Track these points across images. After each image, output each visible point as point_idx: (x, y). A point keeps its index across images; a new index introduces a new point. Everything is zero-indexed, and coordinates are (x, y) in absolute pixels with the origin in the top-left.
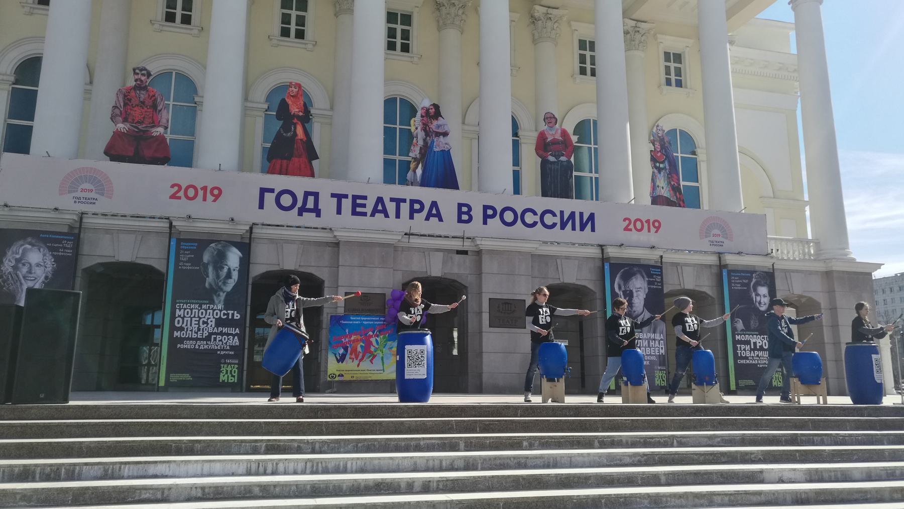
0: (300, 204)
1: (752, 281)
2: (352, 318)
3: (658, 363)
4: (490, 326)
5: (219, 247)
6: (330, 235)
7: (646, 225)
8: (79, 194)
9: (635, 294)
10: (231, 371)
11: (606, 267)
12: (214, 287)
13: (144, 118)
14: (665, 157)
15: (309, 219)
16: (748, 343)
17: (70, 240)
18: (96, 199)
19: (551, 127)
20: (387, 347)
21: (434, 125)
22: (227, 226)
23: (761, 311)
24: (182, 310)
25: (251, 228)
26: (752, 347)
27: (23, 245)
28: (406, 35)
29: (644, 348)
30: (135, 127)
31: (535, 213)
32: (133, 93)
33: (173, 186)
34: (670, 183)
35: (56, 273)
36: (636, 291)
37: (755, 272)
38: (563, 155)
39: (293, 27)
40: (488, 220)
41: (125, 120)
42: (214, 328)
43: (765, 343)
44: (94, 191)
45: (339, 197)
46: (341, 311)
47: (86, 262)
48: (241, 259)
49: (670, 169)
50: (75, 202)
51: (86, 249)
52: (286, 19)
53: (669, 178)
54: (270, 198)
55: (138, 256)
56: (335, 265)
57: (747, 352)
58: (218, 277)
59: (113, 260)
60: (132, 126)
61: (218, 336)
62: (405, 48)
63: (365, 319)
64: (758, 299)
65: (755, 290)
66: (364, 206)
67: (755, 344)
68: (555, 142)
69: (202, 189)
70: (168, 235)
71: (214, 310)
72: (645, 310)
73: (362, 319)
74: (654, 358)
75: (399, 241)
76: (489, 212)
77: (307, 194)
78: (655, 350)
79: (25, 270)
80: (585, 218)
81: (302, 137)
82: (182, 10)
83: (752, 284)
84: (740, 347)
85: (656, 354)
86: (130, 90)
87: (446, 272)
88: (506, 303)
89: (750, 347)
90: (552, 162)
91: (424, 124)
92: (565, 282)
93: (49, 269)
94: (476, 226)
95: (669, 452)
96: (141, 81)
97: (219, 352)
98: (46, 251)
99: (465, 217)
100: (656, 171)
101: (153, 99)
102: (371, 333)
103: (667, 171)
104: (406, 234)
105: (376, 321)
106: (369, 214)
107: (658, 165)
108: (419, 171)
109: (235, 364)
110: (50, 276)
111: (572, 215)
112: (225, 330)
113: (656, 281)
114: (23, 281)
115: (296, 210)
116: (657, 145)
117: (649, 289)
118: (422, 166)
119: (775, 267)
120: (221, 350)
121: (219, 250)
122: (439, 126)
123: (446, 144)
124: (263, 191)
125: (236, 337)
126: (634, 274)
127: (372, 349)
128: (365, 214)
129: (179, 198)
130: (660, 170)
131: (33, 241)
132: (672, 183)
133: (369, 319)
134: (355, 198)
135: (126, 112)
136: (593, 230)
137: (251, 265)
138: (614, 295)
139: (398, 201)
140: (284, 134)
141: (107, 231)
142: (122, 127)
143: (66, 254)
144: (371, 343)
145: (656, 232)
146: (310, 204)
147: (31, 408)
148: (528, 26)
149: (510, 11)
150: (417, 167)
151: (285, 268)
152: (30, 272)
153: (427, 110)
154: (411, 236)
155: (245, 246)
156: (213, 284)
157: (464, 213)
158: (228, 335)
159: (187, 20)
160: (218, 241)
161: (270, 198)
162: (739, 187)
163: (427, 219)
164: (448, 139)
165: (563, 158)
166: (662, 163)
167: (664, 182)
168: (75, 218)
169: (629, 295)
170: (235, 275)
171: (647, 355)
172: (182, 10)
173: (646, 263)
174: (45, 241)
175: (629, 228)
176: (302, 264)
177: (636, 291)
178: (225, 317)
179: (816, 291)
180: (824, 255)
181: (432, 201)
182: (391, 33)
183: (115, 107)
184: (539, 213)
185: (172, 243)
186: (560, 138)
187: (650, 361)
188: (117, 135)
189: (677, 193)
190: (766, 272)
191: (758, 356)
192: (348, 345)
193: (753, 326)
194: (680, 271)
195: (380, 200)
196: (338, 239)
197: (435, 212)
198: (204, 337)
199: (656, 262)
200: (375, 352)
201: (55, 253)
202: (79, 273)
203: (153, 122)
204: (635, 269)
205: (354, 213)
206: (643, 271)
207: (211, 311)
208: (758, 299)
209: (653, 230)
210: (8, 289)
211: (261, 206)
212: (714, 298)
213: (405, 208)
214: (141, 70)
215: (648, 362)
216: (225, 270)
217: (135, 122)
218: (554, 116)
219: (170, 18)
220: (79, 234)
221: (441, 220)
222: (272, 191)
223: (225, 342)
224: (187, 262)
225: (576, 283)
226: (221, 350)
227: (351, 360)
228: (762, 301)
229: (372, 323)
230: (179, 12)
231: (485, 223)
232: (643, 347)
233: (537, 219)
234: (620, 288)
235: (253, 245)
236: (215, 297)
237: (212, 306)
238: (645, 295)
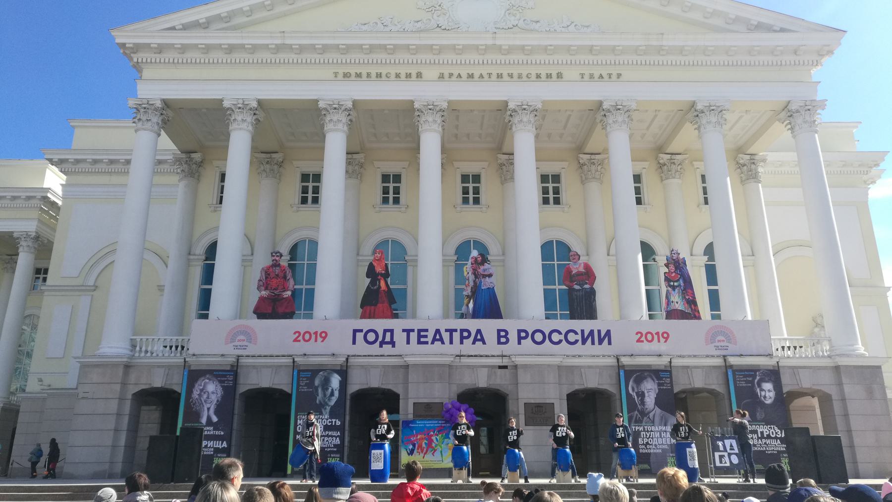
0: (380, 339)
1: (755, 378)
2: (418, 422)
3: (670, 451)
4: (526, 425)
5: (326, 374)
6: (402, 360)
7: (656, 337)
8: (237, 343)
9: (646, 395)
11: (621, 373)
12: (323, 403)
13: (278, 286)
14: (679, 276)
15: (387, 349)
16: (755, 432)
17: (232, 375)
19: (575, 262)
20: (445, 443)
21: (481, 269)
22: (330, 359)
23: (767, 404)
24: (302, 420)
25: (347, 359)
26: (760, 436)
27: (204, 380)
28: (556, 191)
29: (656, 439)
30: (273, 293)
31: (560, 333)
32: (271, 269)
34: (685, 298)
35: (223, 397)
36: (648, 392)
37: (759, 370)
38: (586, 284)
39: (310, 195)
40: (522, 341)
41: (266, 289)
42: (322, 432)
43: (772, 432)
44: (725, 341)
45: (408, 332)
46: (411, 417)
47: (242, 389)
48: (341, 382)
49: (684, 286)
50: (234, 349)
51: (241, 380)
53: (683, 294)
54: (360, 336)
56: (406, 382)
57: (754, 440)
58: (325, 395)
59: (258, 387)
60: (271, 292)
61: (326, 438)
62: (557, 201)
63: (427, 422)
64: (763, 393)
65: (759, 386)
66: (426, 336)
67: (762, 433)
68: (579, 274)
69: (656, 334)
70: (183, 367)
71: (323, 419)
72: (656, 407)
73: (425, 422)
74: (666, 447)
75: (452, 361)
76: (522, 335)
77: (385, 331)
78: (666, 440)
79: (205, 396)
80: (603, 335)
81: (384, 289)
82: (393, 194)
83: (756, 381)
85: (668, 443)
86: (270, 267)
87: (491, 383)
88: (538, 406)
89: (758, 436)
90: (577, 290)
91: (473, 270)
92: (696, 387)
93: (219, 395)
94: (512, 346)
96: (276, 261)
97: (326, 449)
98: (217, 383)
99: (503, 340)
100: (670, 289)
101: (284, 272)
102: (432, 433)
103: (682, 288)
104: (457, 356)
105: (435, 423)
106: (430, 343)
107: (672, 283)
108: (471, 305)
109: (337, 457)
110: (220, 399)
111: (592, 332)
112: (330, 433)
113: (665, 383)
114: (204, 404)
115: (378, 343)
116: (672, 267)
117: (659, 389)
118: (473, 301)
119: (780, 364)
120: (327, 448)
121: (325, 376)
122: (485, 270)
123: (491, 283)
124: (355, 331)
125: (338, 438)
126: (645, 378)
127: (433, 445)
128: (426, 343)
129: (299, 341)
130: (674, 288)
132: (687, 297)
133: (430, 422)
134: (419, 331)
135: (267, 283)
136: (610, 343)
137: (237, 385)
138: (628, 395)
139: (451, 331)
140: (372, 288)
141: (254, 367)
142: (264, 293)
144: (432, 441)
145: (665, 342)
146: (388, 339)
147: (182, 485)
148: (656, 170)
149: (632, 161)
150: (469, 302)
151: (372, 387)
152: (208, 398)
153: (476, 259)
154: (504, 358)
155: (344, 372)
156: (322, 401)
157: (502, 336)
158: (332, 436)
160: (325, 370)
161: (360, 336)
162: (743, 299)
163: (474, 343)
164: (492, 279)
165: (587, 286)
166: (676, 281)
167: (679, 297)
168: (234, 360)
169: (642, 395)
170: (336, 394)
171: (659, 444)
172: (393, 194)
173: (657, 368)
174: (217, 376)
176: (384, 383)
177: (648, 392)
178: (330, 424)
179: (826, 383)
180: (835, 351)
181: (480, 330)
182: (545, 191)
183: (260, 280)
184: (564, 333)
185: (295, 373)
186: (584, 270)
187: (662, 449)
188: (262, 299)
189: (692, 306)
190: (769, 370)
191: (765, 443)
192: (415, 442)
193: (760, 417)
194: (690, 373)
195: (438, 331)
196: (515, 364)
197: (479, 337)
198: (645, 443)
199: (665, 366)
200: (436, 447)
201: (223, 384)
202: (237, 397)
203: (284, 288)
204: (646, 374)
205: (419, 342)
206: (653, 375)
207: (321, 420)
208: (763, 393)
209: (662, 340)
210: (196, 409)
211: (354, 343)
212: (723, 394)
213: (457, 336)
214: (276, 253)
215: (660, 451)
216: (330, 390)
217: (273, 289)
218: (577, 253)
220: (237, 370)
221: (484, 343)
222: (361, 331)
223: (330, 442)
224: (305, 386)
226: (327, 448)
227: (418, 454)
228: (767, 396)
229: (429, 425)
231: (519, 343)
232: (655, 438)
233: (562, 337)
234: (633, 390)
235: (350, 371)
236: (323, 410)
237: (321, 416)
238: (655, 395)
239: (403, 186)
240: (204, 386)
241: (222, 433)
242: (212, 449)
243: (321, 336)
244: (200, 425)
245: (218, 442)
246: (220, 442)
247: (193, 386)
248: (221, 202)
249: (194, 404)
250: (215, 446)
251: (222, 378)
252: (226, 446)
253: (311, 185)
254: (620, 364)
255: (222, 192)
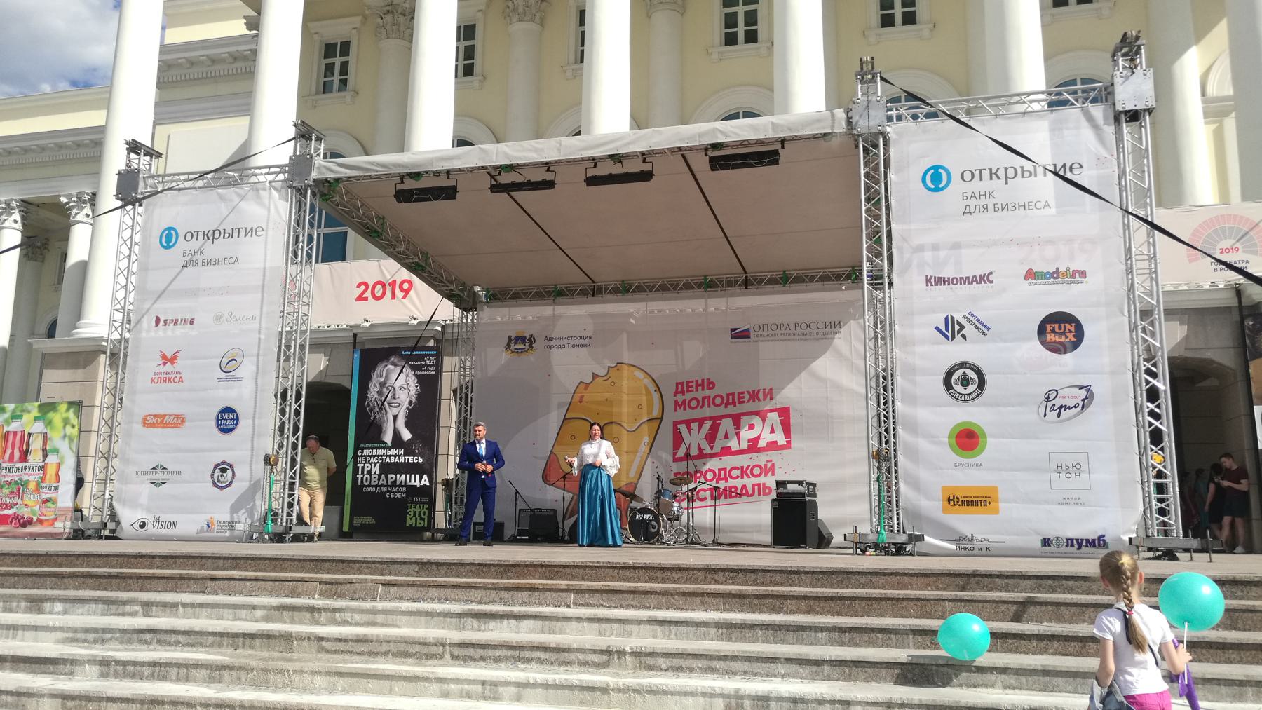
10: (420, 512)
17: (432, 355)
18: (1247, 262)
33: (359, 286)
35: (420, 396)
39: (741, 29)
44: (1241, 250)
52: (730, 21)
55: (328, 374)
69: (390, 284)
84: (363, 468)
93: (413, 392)
95: (1229, 661)
109: (424, 503)
110: (414, 400)
114: (388, 408)
129: (366, 299)
131: (396, 360)
143: (429, 373)
159: (910, 19)
175: (364, 296)
201: (418, 373)
210: (375, 418)
219: (887, 21)
225: (1187, 355)
230: (898, 11)
239: (352, 59)
240: (387, 377)
241: (420, 460)
242: (404, 489)
243: (401, 289)
244: (383, 445)
245: (413, 476)
246: (418, 476)
247: (370, 378)
248: (582, 61)
249: (371, 410)
250: (408, 483)
251: (418, 361)
252: (428, 484)
253: (337, 61)
254: (1245, 302)
255: (582, 44)
